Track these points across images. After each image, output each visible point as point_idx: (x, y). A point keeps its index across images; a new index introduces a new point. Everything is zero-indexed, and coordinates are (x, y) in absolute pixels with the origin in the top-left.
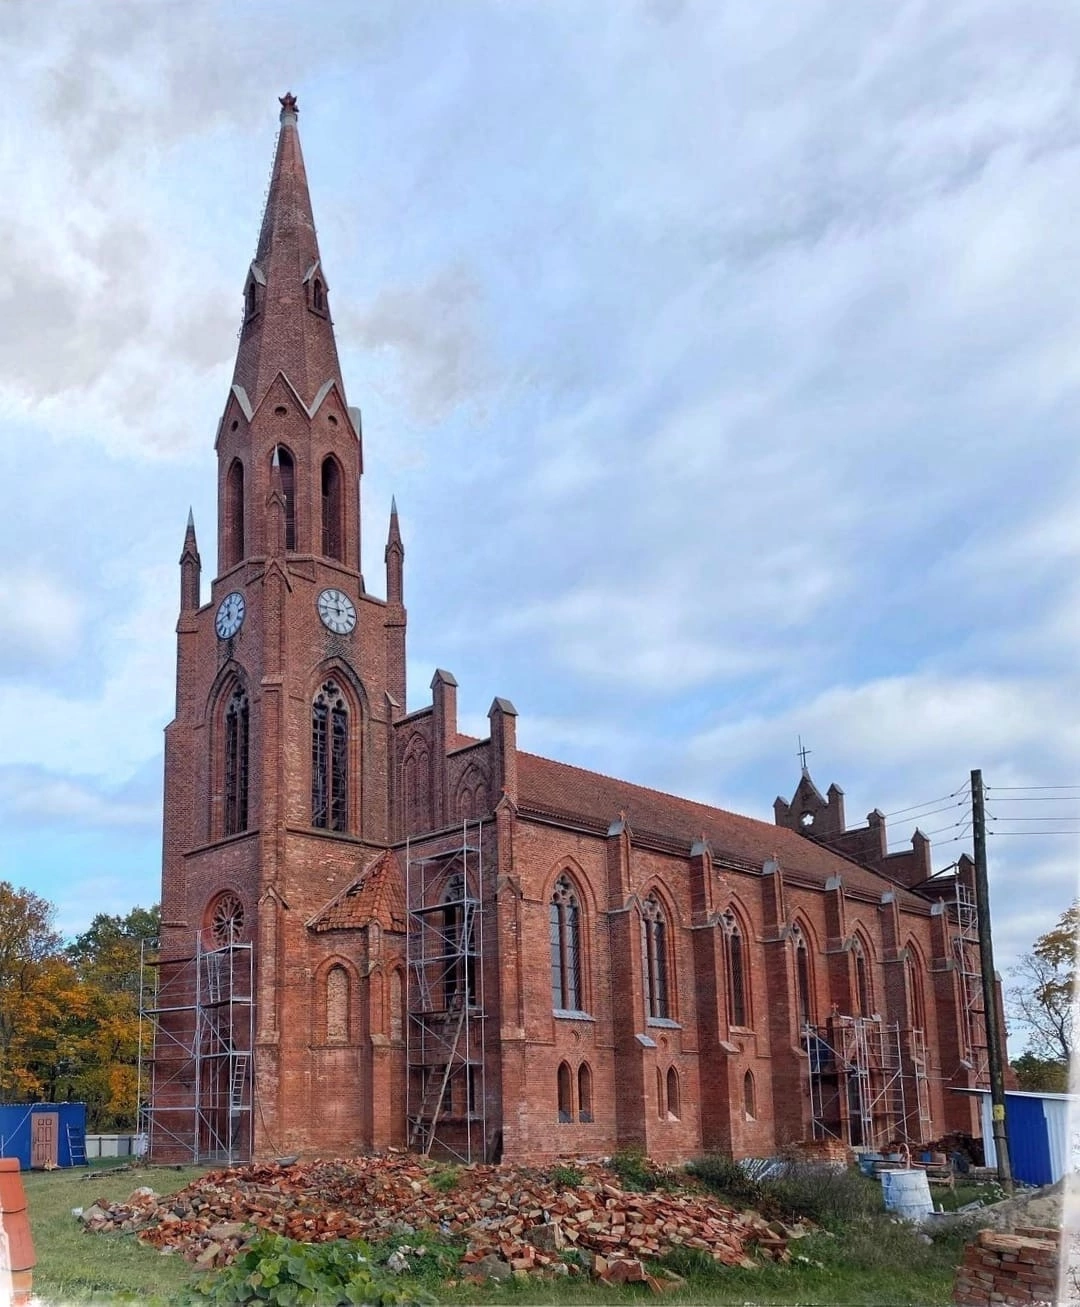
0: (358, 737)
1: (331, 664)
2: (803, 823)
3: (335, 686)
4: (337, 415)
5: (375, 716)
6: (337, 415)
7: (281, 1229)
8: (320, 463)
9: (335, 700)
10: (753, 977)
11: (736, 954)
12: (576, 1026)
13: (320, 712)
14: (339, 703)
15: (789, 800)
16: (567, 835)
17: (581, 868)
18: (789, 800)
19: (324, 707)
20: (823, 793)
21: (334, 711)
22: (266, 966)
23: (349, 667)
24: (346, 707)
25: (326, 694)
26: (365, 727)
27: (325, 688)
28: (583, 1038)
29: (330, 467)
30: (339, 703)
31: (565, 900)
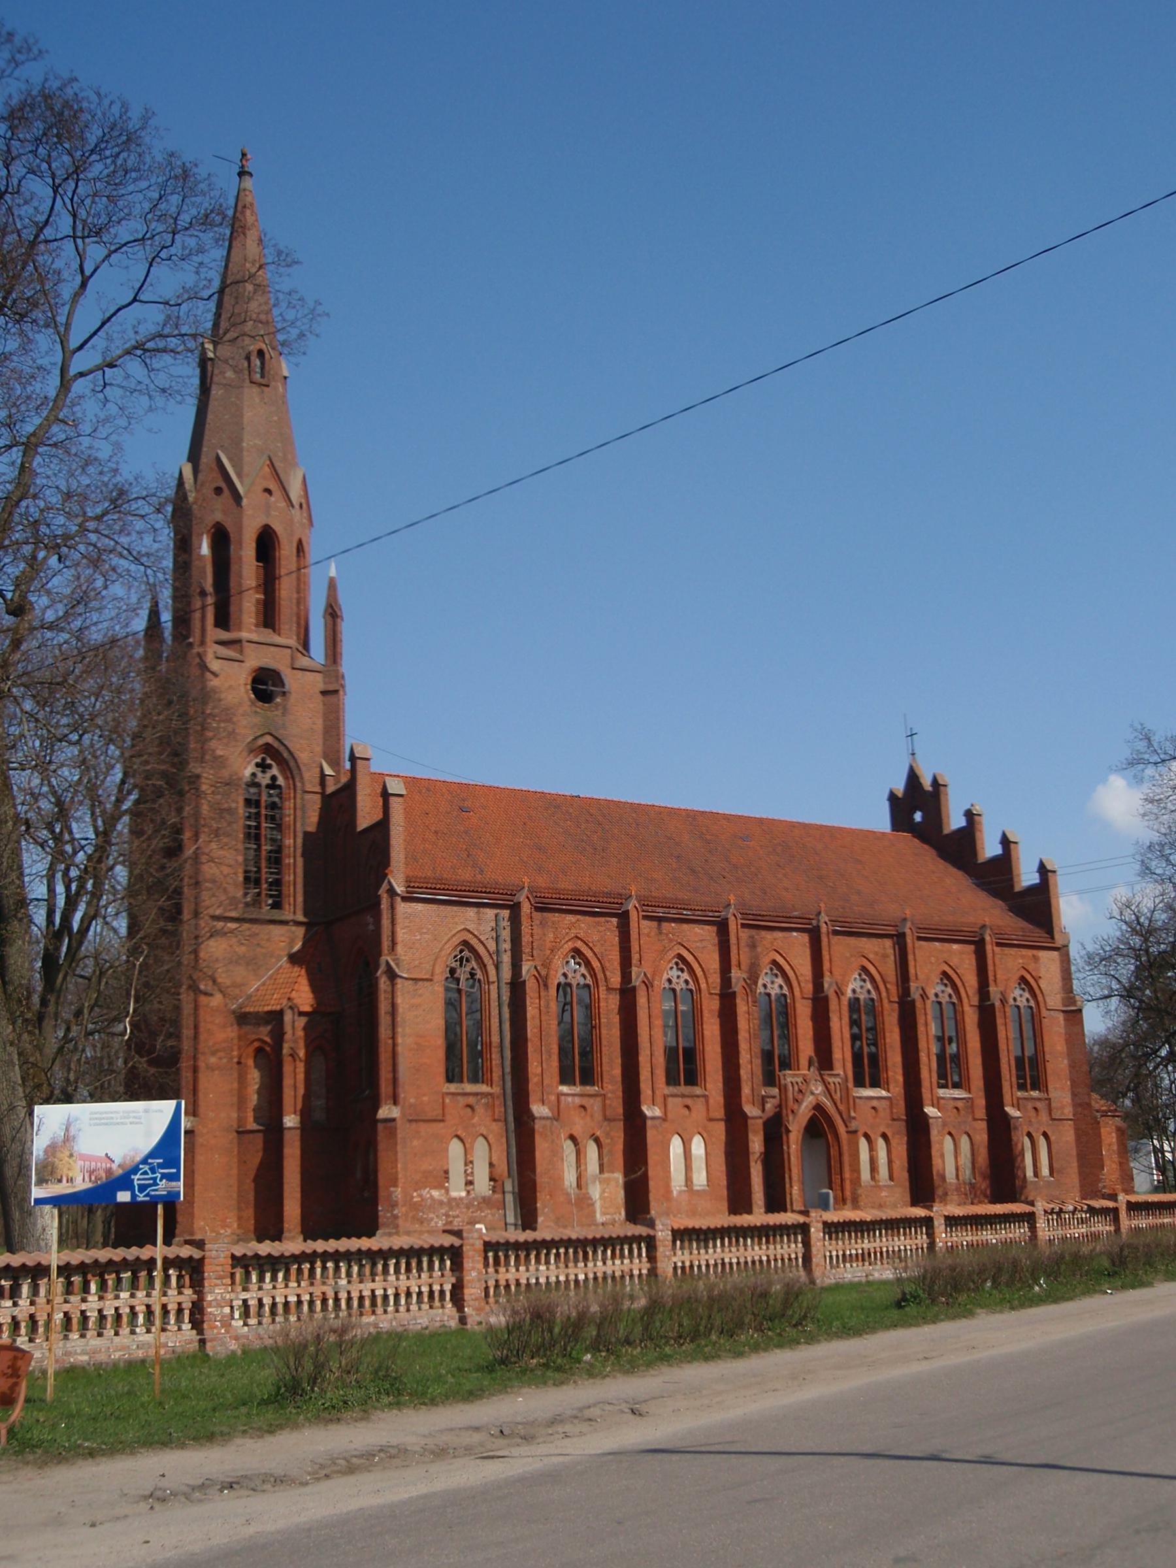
0: (292, 812)
1: (261, 742)
2: (919, 823)
3: (269, 761)
4: (272, 486)
5: (309, 788)
6: (272, 486)
7: (42, 323)
8: (254, 537)
9: (268, 775)
10: (705, 1032)
11: (786, 1014)
12: (471, 1100)
13: (253, 790)
14: (274, 778)
15: (900, 794)
16: (463, 909)
17: (479, 940)
18: (900, 794)
19: (258, 785)
20: (927, 783)
21: (268, 786)
22: (229, 1231)
23: (279, 741)
24: (280, 781)
25: (258, 771)
26: (298, 801)
27: (257, 765)
28: (480, 1110)
29: (266, 543)
30: (274, 778)
31: (463, 974)
